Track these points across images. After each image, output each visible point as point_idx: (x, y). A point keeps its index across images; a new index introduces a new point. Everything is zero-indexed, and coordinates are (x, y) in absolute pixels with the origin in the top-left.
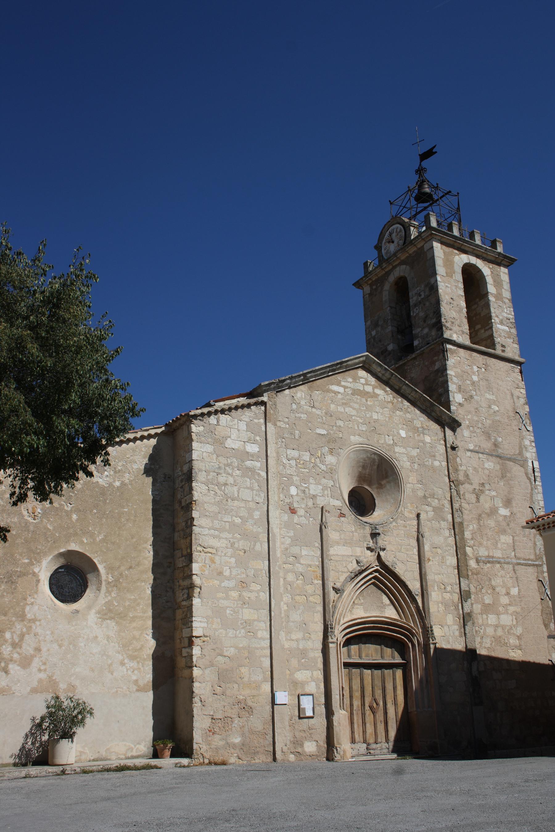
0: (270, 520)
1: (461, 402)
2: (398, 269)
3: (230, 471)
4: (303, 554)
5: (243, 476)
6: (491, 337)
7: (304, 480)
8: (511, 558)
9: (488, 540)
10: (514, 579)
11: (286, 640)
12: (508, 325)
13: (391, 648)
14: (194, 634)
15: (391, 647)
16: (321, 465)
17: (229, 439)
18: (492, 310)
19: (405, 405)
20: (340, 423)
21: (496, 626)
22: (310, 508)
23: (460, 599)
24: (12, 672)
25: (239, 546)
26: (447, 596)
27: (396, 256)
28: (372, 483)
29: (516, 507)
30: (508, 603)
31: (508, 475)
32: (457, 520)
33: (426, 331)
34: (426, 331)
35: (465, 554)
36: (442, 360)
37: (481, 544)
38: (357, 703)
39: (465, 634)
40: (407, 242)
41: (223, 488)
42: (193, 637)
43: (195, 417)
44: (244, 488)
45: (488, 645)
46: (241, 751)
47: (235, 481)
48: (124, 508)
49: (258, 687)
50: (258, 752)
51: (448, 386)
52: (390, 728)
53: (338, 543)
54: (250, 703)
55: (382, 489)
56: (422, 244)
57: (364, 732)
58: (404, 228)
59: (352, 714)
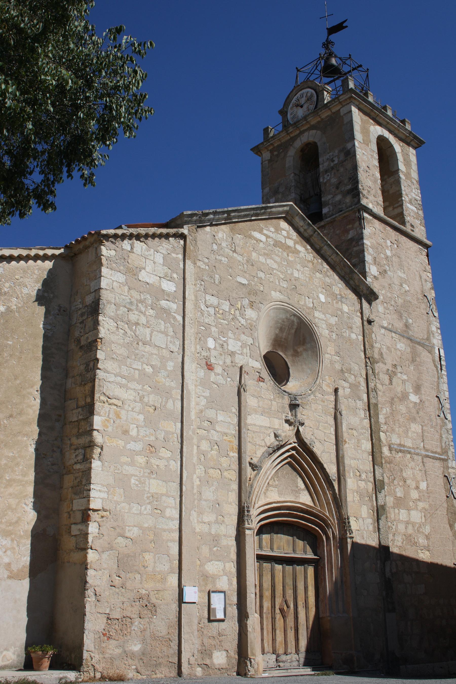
0: (185, 373)
1: (376, 275)
2: (306, 134)
3: (143, 309)
4: (218, 420)
8: (420, 449)
9: (400, 427)
10: (423, 472)
11: (198, 522)
12: (416, 206)
13: (303, 540)
14: (91, 507)
15: (303, 540)
16: (240, 319)
17: (143, 271)
18: (403, 187)
19: (324, 268)
20: (261, 275)
21: (407, 523)
22: (227, 366)
23: (374, 490)
25: (148, 400)
26: (362, 484)
27: (306, 120)
28: (290, 347)
29: (424, 394)
30: (418, 498)
31: (418, 359)
32: (373, 401)
33: (339, 197)
34: (339, 197)
35: (380, 440)
36: (358, 229)
37: (393, 430)
38: (267, 604)
39: (379, 529)
40: (319, 106)
41: (134, 327)
42: (90, 510)
43: (107, 237)
44: (157, 331)
45: (399, 544)
46: (141, 662)
47: (147, 322)
48: (8, 341)
49: (164, 580)
50: (160, 664)
51: (364, 256)
52: (300, 637)
53: (256, 412)
54: (154, 600)
55: (298, 357)
56: (337, 108)
57: (274, 640)
58: (316, 92)
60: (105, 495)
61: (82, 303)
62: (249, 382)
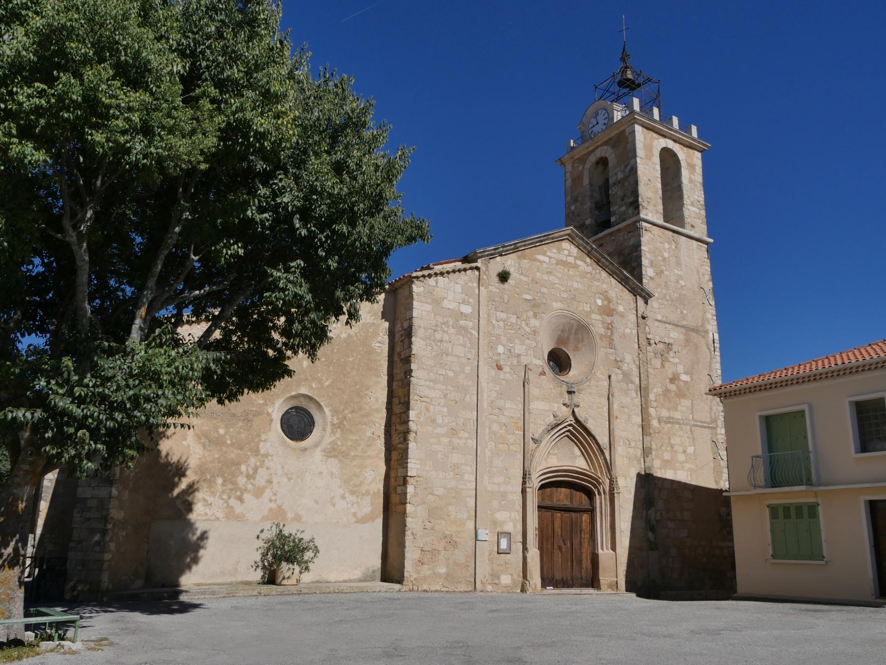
2: (599, 149)
3: (446, 329)
20: (544, 290)
33: (623, 208)
34: (623, 208)
43: (417, 278)
53: (537, 399)
54: (455, 539)
61: (402, 327)
62: (532, 376)
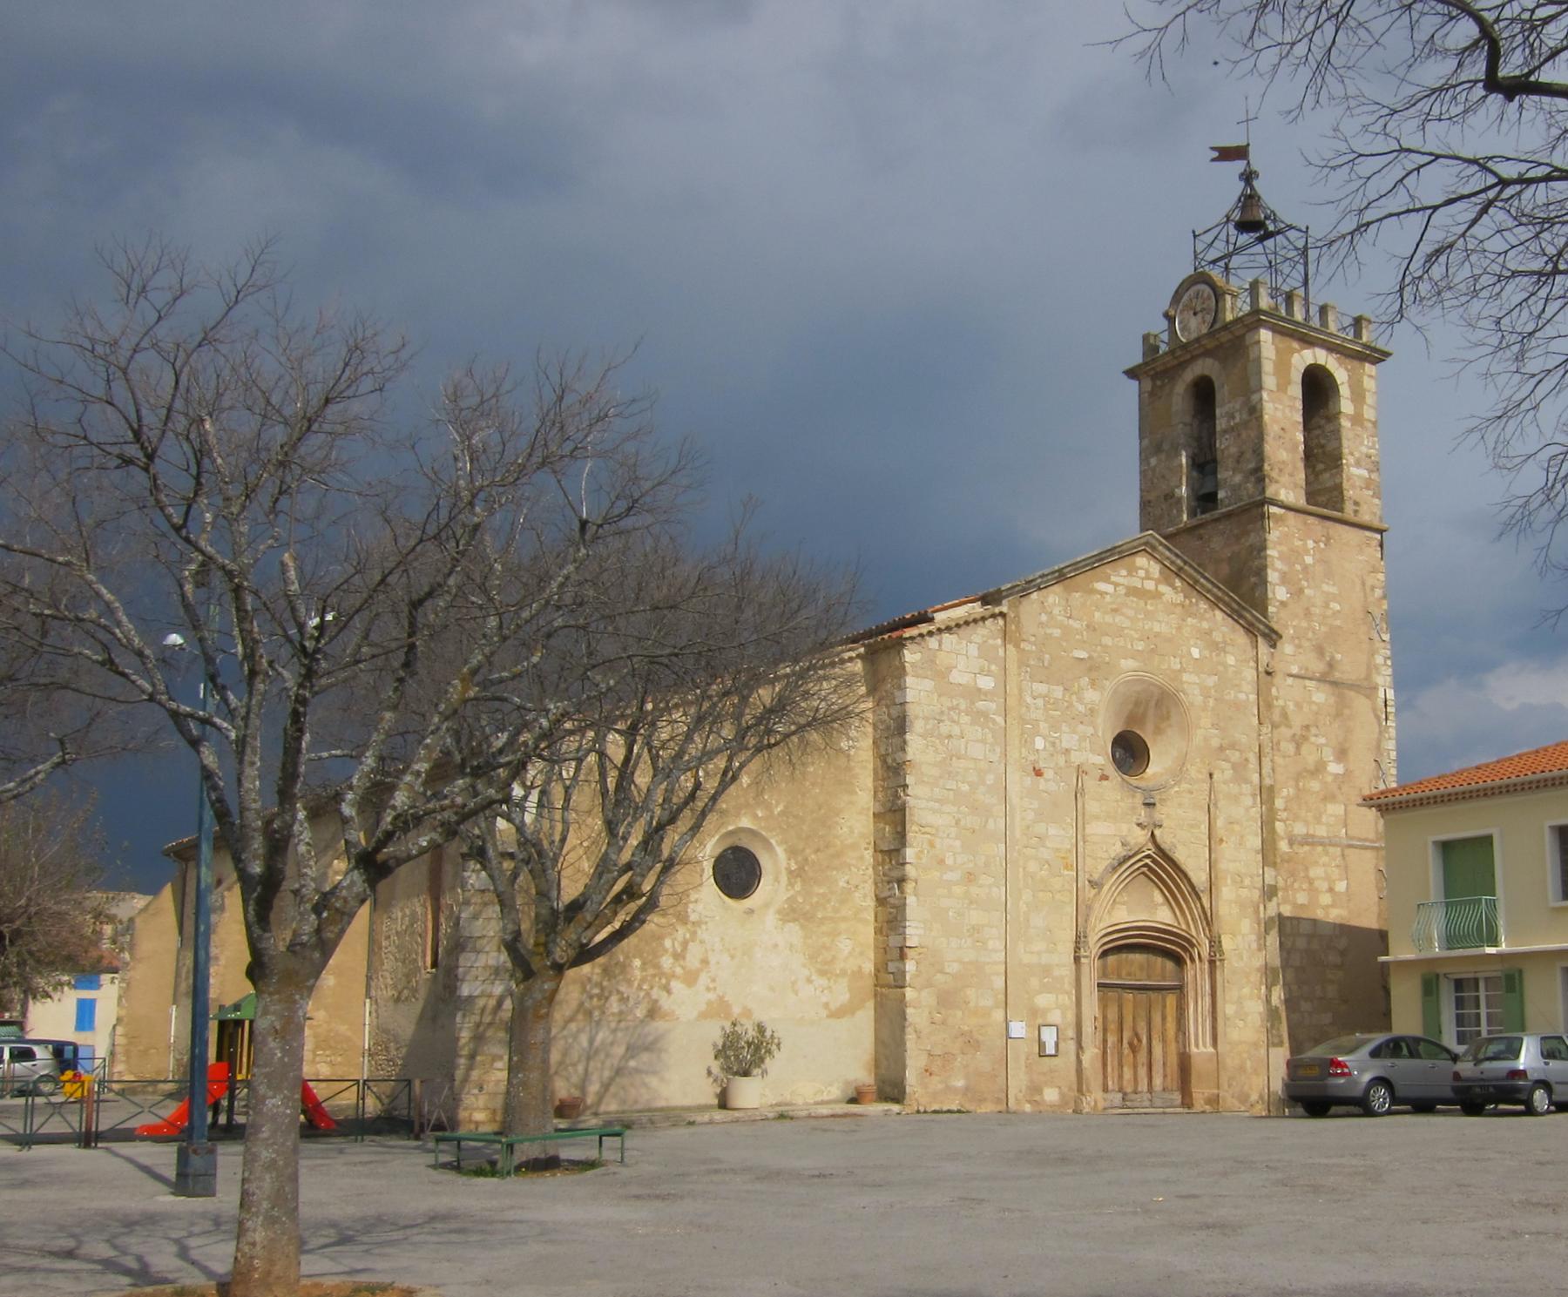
2: (1200, 362)
5: (973, 723)
6: (1339, 488)
7: (1055, 727)
18: (1345, 443)
20: (1107, 641)
24: (674, 991)
26: (1244, 893)
31: (1347, 712)
33: (1238, 478)
38: (1112, 1039)
53: (1097, 818)
59: (1104, 1053)
60: (921, 932)
